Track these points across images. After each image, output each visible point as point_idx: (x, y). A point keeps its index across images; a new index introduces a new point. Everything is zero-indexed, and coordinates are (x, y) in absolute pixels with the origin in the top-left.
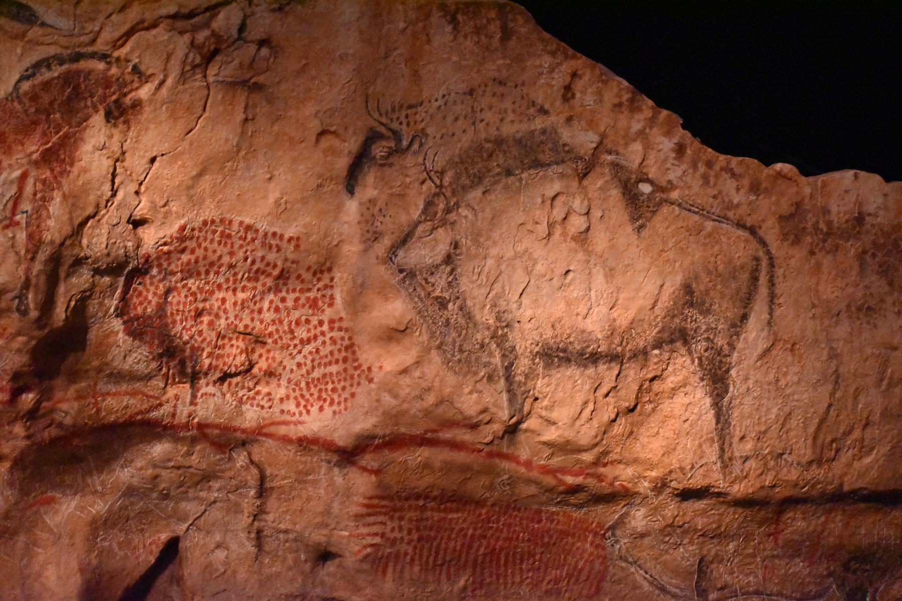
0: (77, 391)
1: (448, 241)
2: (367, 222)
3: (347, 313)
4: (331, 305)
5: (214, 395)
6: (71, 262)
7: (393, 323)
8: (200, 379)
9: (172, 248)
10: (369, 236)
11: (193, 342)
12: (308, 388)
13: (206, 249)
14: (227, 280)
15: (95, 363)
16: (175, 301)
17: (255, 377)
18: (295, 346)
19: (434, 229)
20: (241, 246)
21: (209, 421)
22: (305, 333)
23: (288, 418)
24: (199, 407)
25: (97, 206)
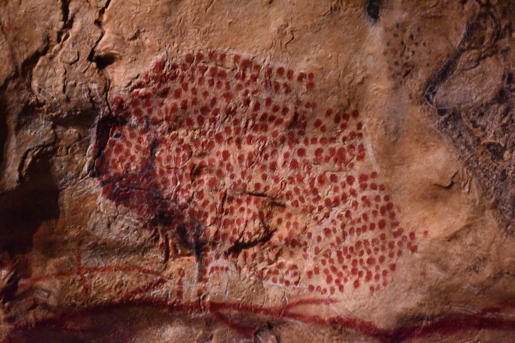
0: (56, 267)
1: (500, 72)
2: (395, 52)
3: (381, 167)
4: (361, 158)
5: (227, 269)
6: (19, 109)
7: (435, 178)
8: (206, 250)
9: (150, 90)
10: (398, 69)
11: (192, 206)
12: (341, 260)
13: (194, 91)
14: (228, 130)
15: (73, 233)
16: (164, 156)
17: (275, 247)
18: (321, 209)
19: (480, 59)
20: (239, 87)
21: (224, 300)
22: (331, 192)
23: (318, 295)
24: (209, 284)
25: (47, 40)
